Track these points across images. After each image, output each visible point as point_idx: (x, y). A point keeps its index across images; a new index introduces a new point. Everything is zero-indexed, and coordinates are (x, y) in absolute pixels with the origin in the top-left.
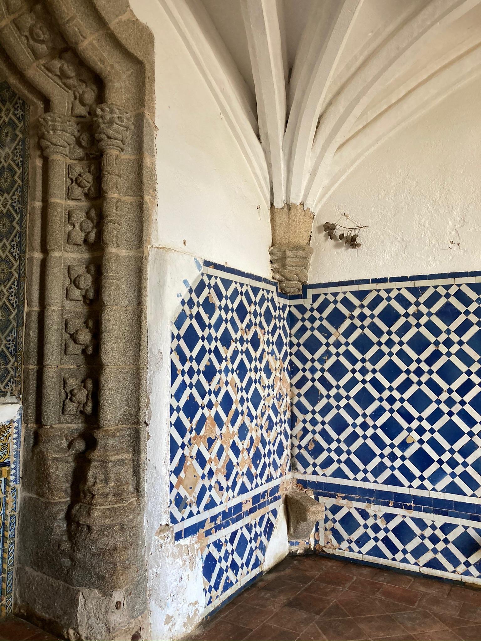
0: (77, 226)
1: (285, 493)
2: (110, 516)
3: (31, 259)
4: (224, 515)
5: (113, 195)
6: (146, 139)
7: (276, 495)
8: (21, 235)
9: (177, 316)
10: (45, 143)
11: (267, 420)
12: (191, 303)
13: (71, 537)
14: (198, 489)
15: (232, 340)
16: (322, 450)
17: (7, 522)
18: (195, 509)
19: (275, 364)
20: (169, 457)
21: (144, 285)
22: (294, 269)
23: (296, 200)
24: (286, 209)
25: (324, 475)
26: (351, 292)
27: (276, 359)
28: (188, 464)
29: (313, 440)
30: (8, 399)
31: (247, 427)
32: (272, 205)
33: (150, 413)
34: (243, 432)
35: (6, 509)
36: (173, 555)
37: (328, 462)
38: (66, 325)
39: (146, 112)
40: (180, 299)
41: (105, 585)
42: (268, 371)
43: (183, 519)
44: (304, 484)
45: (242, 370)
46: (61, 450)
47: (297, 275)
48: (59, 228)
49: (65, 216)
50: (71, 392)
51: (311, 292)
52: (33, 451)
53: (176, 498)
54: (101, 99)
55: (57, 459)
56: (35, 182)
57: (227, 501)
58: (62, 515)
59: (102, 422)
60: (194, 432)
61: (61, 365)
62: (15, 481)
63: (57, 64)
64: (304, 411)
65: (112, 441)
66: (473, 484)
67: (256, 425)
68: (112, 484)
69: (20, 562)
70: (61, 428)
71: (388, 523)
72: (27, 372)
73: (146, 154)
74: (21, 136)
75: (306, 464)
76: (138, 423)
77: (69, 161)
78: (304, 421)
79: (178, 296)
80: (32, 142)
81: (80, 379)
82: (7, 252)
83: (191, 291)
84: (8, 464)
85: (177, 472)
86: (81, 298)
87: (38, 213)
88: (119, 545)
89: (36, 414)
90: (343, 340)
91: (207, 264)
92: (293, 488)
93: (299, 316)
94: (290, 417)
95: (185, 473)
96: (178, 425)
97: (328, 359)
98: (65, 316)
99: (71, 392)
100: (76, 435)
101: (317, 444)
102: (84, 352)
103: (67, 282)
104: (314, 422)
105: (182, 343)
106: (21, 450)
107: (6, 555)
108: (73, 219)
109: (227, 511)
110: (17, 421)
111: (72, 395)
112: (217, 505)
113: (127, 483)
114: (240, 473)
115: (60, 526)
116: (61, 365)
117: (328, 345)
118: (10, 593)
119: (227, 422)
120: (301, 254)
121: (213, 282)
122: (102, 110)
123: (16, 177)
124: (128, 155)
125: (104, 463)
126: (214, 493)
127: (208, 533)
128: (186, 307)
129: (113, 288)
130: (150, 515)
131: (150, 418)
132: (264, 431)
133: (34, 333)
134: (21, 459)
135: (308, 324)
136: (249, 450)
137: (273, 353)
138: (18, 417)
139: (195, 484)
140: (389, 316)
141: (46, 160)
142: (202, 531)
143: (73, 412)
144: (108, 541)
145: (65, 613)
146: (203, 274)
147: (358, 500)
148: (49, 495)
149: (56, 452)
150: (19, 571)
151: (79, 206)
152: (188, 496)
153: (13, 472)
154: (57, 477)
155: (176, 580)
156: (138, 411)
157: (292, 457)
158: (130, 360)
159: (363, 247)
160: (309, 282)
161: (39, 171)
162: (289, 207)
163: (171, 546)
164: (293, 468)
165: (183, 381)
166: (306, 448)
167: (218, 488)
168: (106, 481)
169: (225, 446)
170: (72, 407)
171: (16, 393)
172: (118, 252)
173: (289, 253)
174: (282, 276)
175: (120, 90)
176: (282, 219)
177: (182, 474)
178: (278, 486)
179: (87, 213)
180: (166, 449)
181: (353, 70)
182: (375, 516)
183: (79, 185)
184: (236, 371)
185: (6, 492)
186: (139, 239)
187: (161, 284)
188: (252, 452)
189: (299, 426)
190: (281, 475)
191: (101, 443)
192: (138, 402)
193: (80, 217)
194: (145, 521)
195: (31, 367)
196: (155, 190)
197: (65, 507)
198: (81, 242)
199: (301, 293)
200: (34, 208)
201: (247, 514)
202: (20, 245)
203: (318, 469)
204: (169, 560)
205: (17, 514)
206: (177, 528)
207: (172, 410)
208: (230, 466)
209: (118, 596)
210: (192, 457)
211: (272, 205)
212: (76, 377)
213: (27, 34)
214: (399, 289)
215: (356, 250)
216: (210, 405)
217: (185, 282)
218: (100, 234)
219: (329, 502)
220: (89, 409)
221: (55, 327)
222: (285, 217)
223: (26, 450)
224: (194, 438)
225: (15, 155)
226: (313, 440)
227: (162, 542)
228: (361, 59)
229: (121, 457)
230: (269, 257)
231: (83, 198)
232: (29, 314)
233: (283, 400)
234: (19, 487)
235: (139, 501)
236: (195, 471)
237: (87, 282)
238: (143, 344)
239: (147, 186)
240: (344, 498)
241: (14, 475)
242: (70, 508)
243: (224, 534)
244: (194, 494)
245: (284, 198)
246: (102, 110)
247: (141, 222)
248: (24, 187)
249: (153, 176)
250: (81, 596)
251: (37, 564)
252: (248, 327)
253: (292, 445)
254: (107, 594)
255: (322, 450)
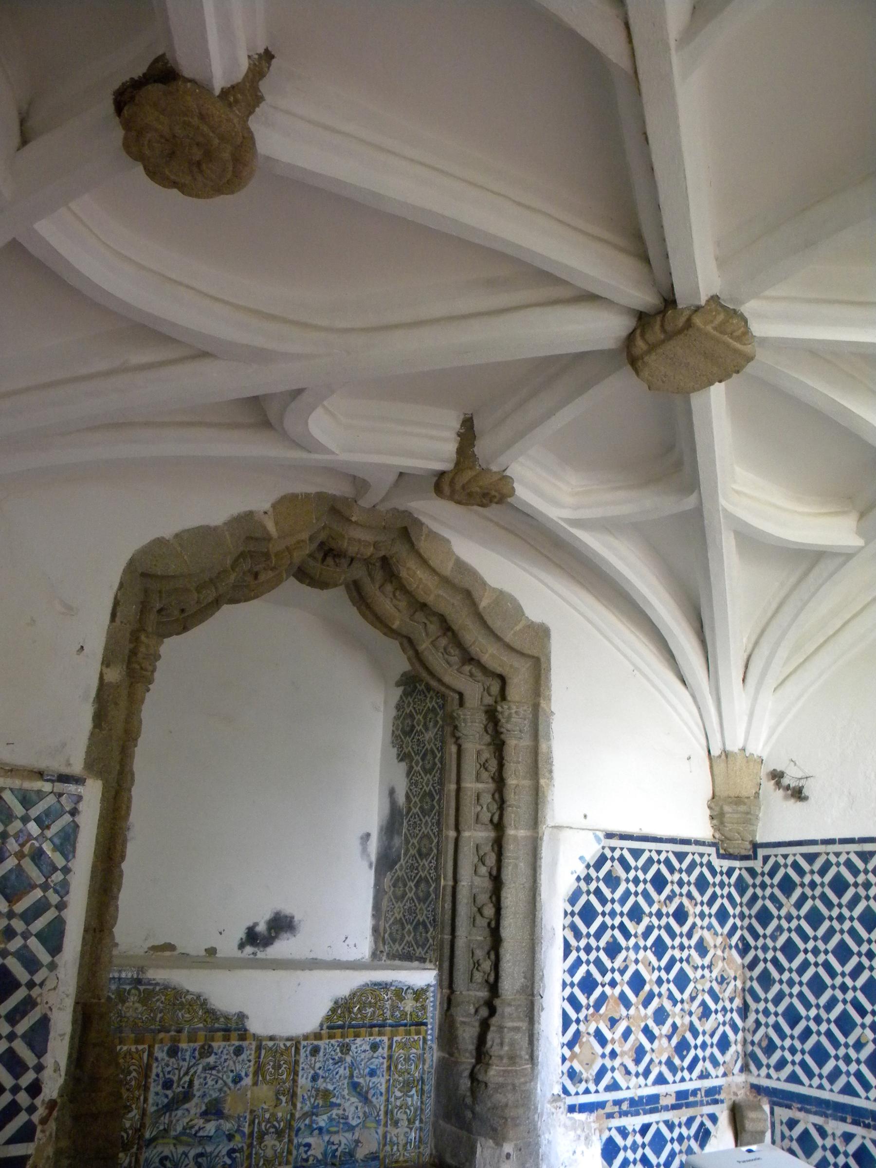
0: (485, 808)
1: (734, 1098)
2: (503, 1076)
3: (447, 837)
4: (632, 1102)
5: (511, 781)
6: (541, 728)
7: (717, 1097)
8: (440, 813)
9: (571, 893)
10: (458, 734)
11: (699, 1006)
12: (588, 879)
13: (473, 1091)
14: (596, 1068)
15: (645, 913)
16: (776, 1047)
17: (425, 1077)
18: (592, 1087)
19: (715, 941)
20: (560, 1029)
21: (538, 863)
22: (735, 826)
23: (733, 747)
24: (723, 756)
25: (778, 1079)
26: (802, 855)
27: (716, 934)
28: (584, 1040)
29: (766, 1035)
30: (428, 965)
31: (666, 1011)
32: (709, 751)
33: (544, 987)
34: (661, 1016)
35: (424, 1064)
36: (565, 1126)
37: (781, 1064)
38: (474, 898)
39: (542, 701)
40: (575, 876)
41: (498, 1137)
42: (702, 948)
43: (577, 1094)
44: (757, 1089)
45: (659, 948)
46: (468, 1015)
47: (739, 833)
48: (469, 810)
49: (474, 797)
50: (478, 961)
51: (761, 852)
52: (446, 1015)
53: (568, 1071)
54: (503, 695)
55: (464, 1023)
56: (450, 766)
57: (637, 1088)
58: (466, 1073)
59: (500, 991)
60: (591, 1010)
61: (470, 936)
62: (432, 1040)
63: (467, 668)
64: (757, 999)
65: (508, 1010)
66: (867, 1086)
67: (682, 1010)
68: (506, 1048)
69: (435, 1116)
70: (469, 995)
71: (847, 1144)
72: (442, 941)
73: (541, 740)
74: (441, 722)
75: (759, 1066)
76: (533, 995)
77: (479, 747)
78: (757, 1012)
79: (572, 873)
80: (448, 729)
81: (486, 951)
82: (428, 829)
83: (588, 866)
84: (425, 1024)
85: (571, 1045)
86: (487, 874)
87: (453, 794)
88: (510, 1103)
89: (448, 981)
90: (794, 913)
91: (610, 836)
92: (746, 1095)
93: (750, 881)
94: (741, 1006)
95: (580, 1047)
96: (572, 1000)
97: (781, 934)
98: (474, 891)
99: (478, 961)
100: (482, 1002)
101: (771, 1041)
102: (489, 924)
103: (476, 859)
104: (766, 1013)
105: (578, 920)
106: (437, 1012)
107: (423, 1107)
108: (481, 801)
109: (636, 1099)
110: (434, 986)
111: (479, 965)
112: (622, 1089)
113: (521, 1049)
114: (657, 1061)
115: (465, 1083)
116: (470, 936)
117: (779, 918)
118: (426, 1143)
119: (638, 1003)
120: (742, 808)
121: (617, 854)
122: (502, 707)
123: (436, 760)
124: (526, 742)
125: (501, 1028)
126: (619, 1076)
127: (610, 1116)
128: (583, 884)
129: (510, 868)
130: (543, 1084)
131: (544, 991)
132: (695, 1019)
133: (448, 906)
134: (437, 1021)
135: (759, 891)
136: (670, 1038)
137: (710, 927)
138: (434, 982)
139: (593, 1061)
140: (839, 885)
141: (459, 747)
142: (601, 1112)
143: (479, 981)
144: (499, 1098)
145: (467, 1161)
146: (603, 848)
147: (815, 1113)
148: (456, 1055)
149: (463, 1016)
150: (435, 1125)
151: (487, 786)
152: (583, 1071)
153: (429, 1032)
154: (464, 1038)
155: (568, 1151)
156: (533, 983)
157: (745, 1055)
158: (527, 936)
159: (812, 800)
160: (759, 839)
161: (454, 756)
162: (726, 754)
163: (563, 1117)
164: (745, 1069)
165: (578, 957)
166: (759, 1044)
167: (624, 1072)
168: (502, 1044)
169: (633, 1029)
170: (478, 976)
171: (434, 960)
172: (516, 833)
173: (727, 809)
174: (723, 835)
175: (518, 690)
176: (720, 767)
177: (577, 1049)
178: (720, 1087)
179: (493, 795)
180: (558, 1022)
181: (769, 614)
182: (833, 1135)
183: (486, 769)
184: (651, 948)
185: (424, 1049)
186: (535, 821)
187: (554, 863)
188: (675, 1041)
189: (752, 1017)
190: (725, 1075)
191: (499, 1010)
192: (533, 975)
193: (487, 799)
194: (539, 1088)
195: (446, 937)
196: (551, 772)
197: (469, 1067)
198: (488, 822)
199: (751, 853)
200: (449, 790)
201: (666, 1108)
202: (439, 823)
203: (772, 1071)
204: (561, 1130)
205: (433, 1071)
206: (570, 1101)
207: (564, 985)
208: (639, 1053)
209: (508, 1148)
210: (588, 1034)
211: (709, 751)
212: (482, 948)
213: (442, 650)
214: (848, 853)
215: (800, 804)
216: (613, 984)
217: (581, 858)
218: (501, 817)
219: (783, 1114)
220: (492, 979)
221: (465, 901)
222: (723, 765)
223: (440, 1013)
224: (593, 1015)
225: (436, 739)
226: (766, 1035)
227: (553, 1110)
228: (774, 606)
229: (515, 1024)
230: (708, 812)
231: (490, 780)
232: (444, 888)
233: (728, 984)
234: (435, 1046)
235: (533, 1069)
236: (592, 1048)
237: (491, 860)
238: (538, 920)
239: (543, 771)
240: (800, 1110)
241: (430, 1034)
242: (474, 1067)
243: (633, 1123)
244: (591, 1071)
245: (720, 745)
246: (502, 707)
247: (537, 804)
248: (442, 770)
249: (549, 761)
250: (479, 1145)
251: (447, 1117)
252: (670, 898)
253: (745, 1041)
254: (499, 1144)
255: (776, 1047)
